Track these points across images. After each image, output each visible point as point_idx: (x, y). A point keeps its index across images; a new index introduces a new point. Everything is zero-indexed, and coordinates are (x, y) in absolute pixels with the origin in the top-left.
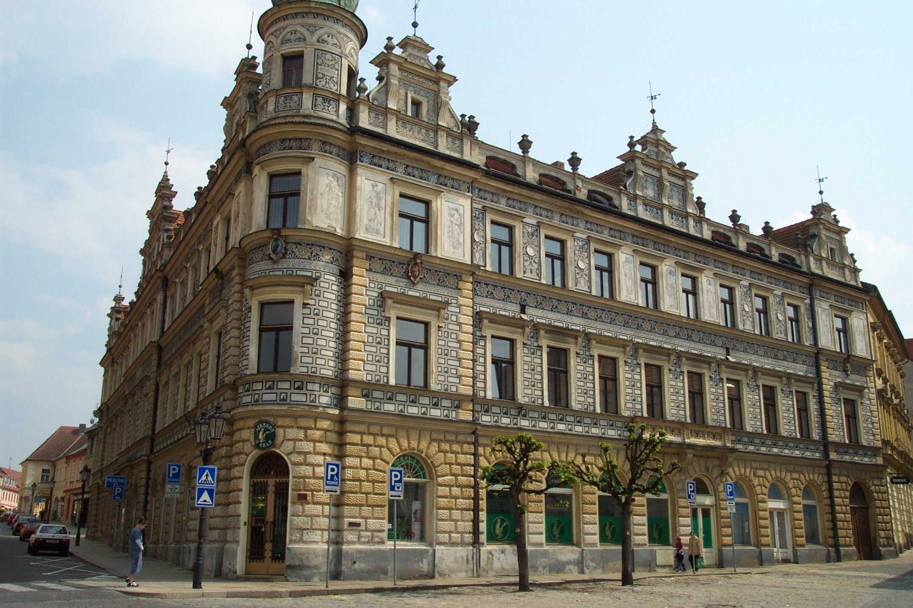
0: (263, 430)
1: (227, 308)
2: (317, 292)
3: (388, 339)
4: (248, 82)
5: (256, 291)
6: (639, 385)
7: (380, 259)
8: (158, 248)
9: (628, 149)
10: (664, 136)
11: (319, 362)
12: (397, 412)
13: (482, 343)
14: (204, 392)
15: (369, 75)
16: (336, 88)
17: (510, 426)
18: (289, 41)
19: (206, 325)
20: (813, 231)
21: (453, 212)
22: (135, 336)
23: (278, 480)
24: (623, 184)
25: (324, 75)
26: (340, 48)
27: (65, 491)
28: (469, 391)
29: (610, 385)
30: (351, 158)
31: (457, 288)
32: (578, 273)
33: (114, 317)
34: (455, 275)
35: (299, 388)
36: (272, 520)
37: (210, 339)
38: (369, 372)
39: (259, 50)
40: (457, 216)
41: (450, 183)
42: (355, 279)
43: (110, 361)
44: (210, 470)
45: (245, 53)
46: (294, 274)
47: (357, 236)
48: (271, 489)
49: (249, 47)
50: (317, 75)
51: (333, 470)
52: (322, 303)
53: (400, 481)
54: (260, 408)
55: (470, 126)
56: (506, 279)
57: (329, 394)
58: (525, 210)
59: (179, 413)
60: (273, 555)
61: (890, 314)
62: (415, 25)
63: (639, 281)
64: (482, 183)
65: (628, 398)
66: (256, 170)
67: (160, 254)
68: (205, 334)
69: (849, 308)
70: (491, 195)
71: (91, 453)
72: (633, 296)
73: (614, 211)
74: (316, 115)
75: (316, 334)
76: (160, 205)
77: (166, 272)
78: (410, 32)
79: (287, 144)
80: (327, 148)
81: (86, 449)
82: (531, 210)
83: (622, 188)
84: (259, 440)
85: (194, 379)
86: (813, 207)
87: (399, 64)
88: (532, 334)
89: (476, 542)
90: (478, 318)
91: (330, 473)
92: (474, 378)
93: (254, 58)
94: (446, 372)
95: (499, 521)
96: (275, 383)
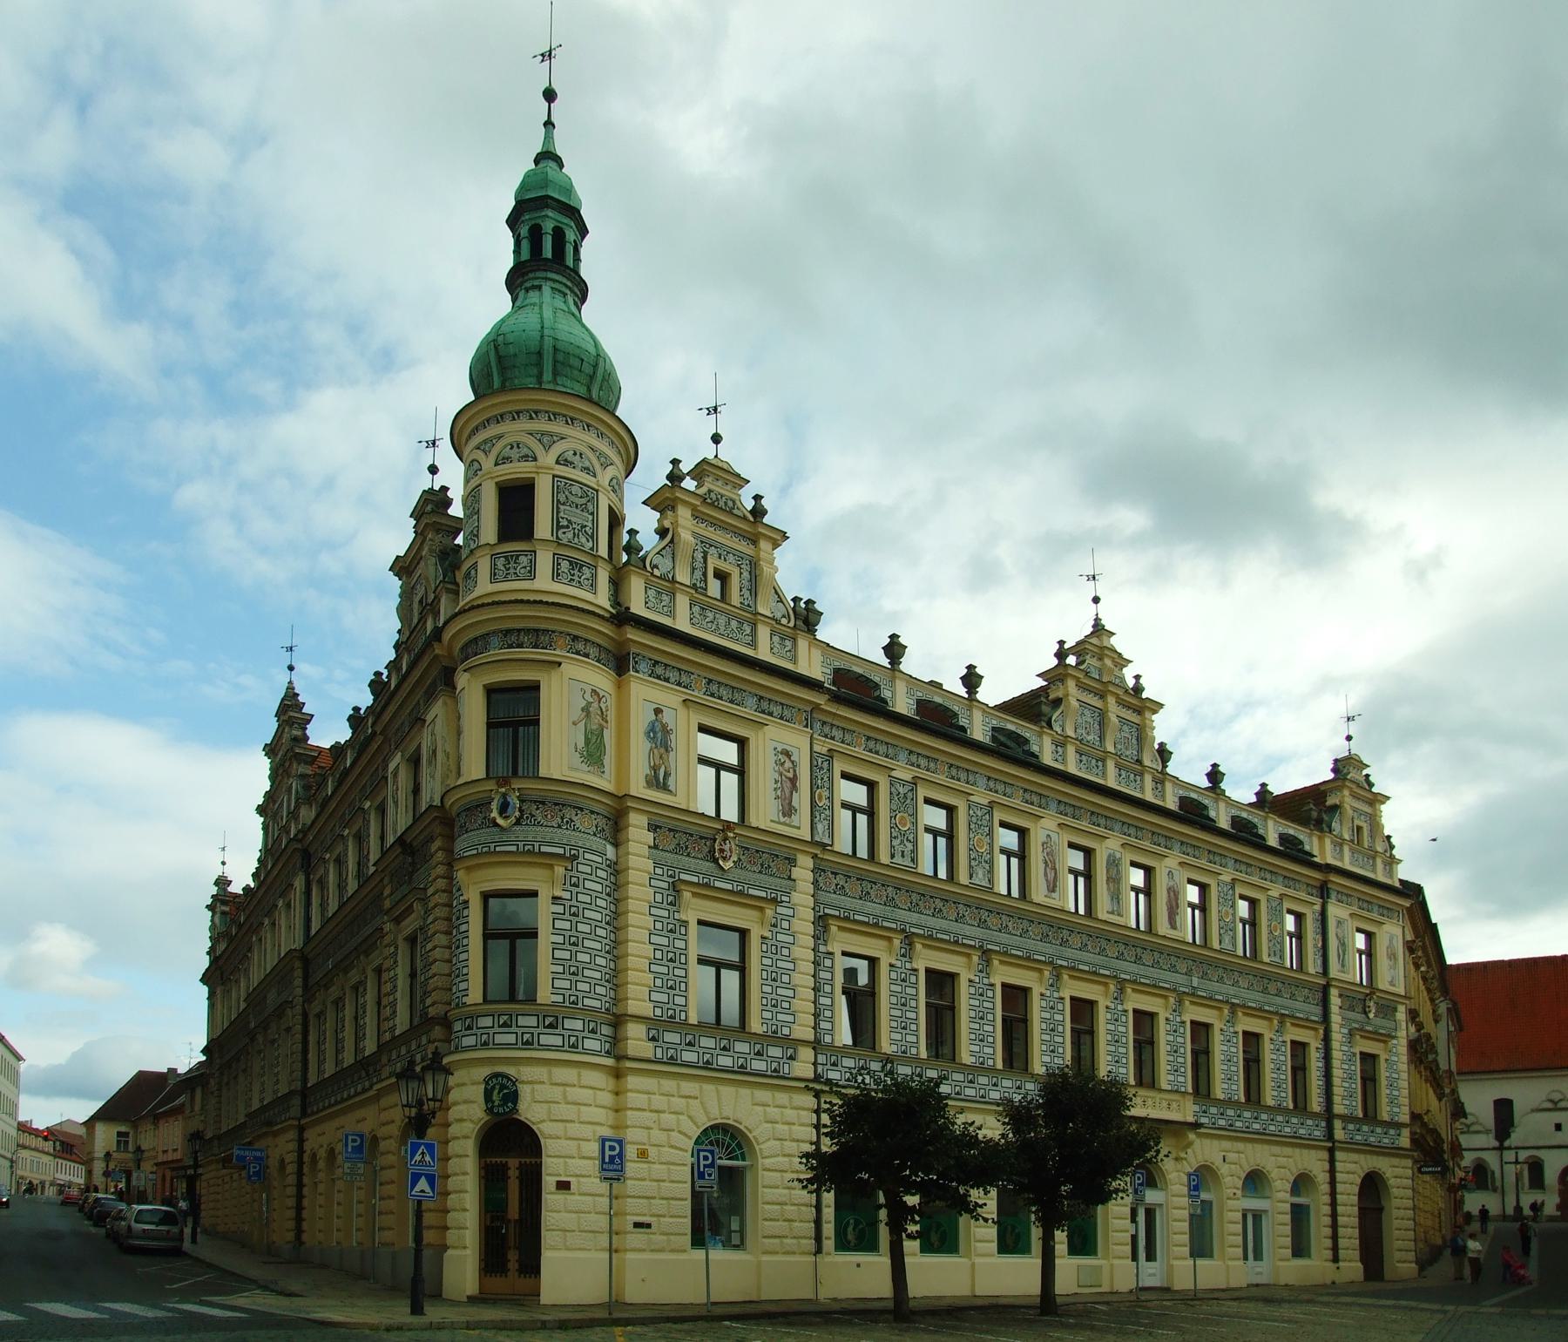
0: (497, 1087)
1: (424, 900)
4: (438, 531)
6: (913, 1003)
9: (1055, 662)
10: (1114, 641)
13: (828, 963)
14: (393, 1028)
15: (642, 522)
16: (590, 544)
17: (840, 1083)
18: (507, 460)
19: (387, 927)
20: (1331, 801)
21: (783, 758)
22: (260, 940)
23: (523, 1160)
24: (1046, 719)
25: (569, 521)
27: (156, 1164)
29: (1202, 1059)
30: (620, 663)
33: (218, 910)
34: (786, 858)
35: (551, 1026)
37: (396, 948)
39: (453, 476)
40: (788, 764)
41: (777, 710)
43: (217, 977)
44: (427, 1146)
45: (426, 482)
46: (537, 850)
48: (513, 1173)
49: (433, 470)
50: (558, 522)
51: (612, 1148)
53: (712, 1165)
55: (807, 617)
59: (348, 1059)
61: (1433, 930)
62: (716, 439)
64: (826, 711)
67: (294, 815)
68: (387, 939)
69: (1379, 918)
70: (841, 732)
73: (1031, 762)
76: (285, 735)
78: (709, 451)
80: (580, 646)
81: (183, 1105)
82: (903, 756)
86: (1336, 761)
87: (694, 509)
88: (903, 950)
89: (819, 1250)
91: (608, 1153)
93: (444, 489)
95: (852, 1221)
96: (514, 1018)
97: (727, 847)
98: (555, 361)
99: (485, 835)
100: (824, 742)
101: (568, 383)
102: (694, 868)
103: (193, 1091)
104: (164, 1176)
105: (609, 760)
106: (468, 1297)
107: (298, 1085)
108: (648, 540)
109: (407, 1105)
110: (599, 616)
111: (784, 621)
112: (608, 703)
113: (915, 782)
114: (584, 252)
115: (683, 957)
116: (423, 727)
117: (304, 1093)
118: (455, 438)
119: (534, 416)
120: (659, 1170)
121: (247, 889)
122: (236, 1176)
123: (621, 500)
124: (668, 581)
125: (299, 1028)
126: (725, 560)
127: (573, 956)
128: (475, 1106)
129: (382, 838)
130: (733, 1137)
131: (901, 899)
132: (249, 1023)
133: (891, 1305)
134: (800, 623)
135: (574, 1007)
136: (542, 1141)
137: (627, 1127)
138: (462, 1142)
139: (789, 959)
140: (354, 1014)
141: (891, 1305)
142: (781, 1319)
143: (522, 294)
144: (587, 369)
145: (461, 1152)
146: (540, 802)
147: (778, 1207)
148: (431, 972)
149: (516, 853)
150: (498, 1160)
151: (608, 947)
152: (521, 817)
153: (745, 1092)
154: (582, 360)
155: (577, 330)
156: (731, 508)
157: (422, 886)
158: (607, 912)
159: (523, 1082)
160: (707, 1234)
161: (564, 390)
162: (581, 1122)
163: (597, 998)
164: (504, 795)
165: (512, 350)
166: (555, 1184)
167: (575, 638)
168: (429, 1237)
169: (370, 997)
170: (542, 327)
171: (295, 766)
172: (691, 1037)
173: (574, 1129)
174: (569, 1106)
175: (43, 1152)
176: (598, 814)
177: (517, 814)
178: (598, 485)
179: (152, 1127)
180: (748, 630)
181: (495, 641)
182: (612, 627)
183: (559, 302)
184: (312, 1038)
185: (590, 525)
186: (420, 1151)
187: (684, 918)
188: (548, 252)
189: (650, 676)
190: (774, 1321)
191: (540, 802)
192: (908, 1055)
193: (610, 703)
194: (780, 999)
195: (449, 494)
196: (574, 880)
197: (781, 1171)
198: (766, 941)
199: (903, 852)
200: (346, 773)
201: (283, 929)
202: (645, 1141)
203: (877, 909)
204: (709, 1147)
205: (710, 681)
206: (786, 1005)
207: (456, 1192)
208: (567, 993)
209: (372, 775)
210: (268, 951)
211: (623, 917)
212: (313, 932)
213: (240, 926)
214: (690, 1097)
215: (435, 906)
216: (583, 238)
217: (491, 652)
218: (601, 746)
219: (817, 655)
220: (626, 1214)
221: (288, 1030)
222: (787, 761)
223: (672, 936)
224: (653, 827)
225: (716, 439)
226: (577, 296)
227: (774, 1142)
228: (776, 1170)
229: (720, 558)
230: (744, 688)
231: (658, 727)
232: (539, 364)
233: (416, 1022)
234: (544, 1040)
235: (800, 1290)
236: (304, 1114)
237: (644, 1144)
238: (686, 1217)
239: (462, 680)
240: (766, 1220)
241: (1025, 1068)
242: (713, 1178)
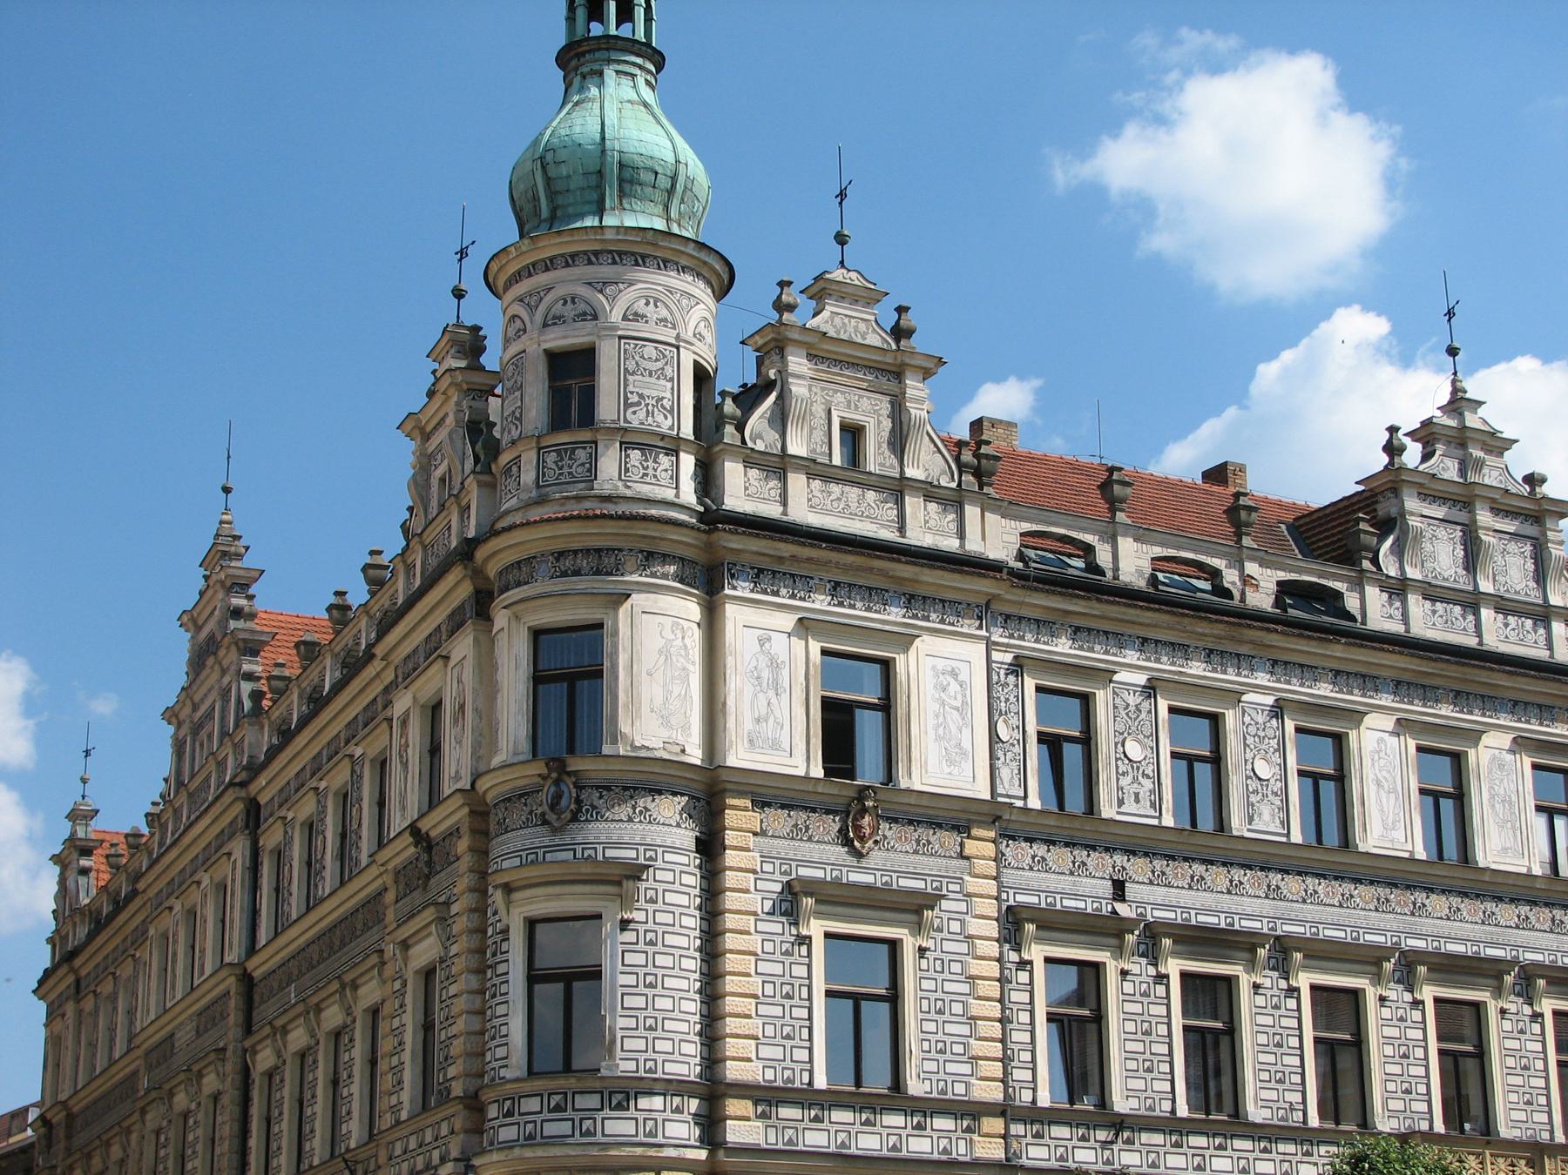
2: (650, 893)
3: (810, 988)
5: (516, 896)
8: (223, 718)
9: (1385, 459)
11: (660, 1045)
12: (833, 1149)
13: (1023, 977)
18: (558, 320)
25: (641, 396)
28: (994, 1093)
29: (1346, 1061)
31: (961, 856)
32: (1256, 792)
37: (404, 984)
38: (769, 1063)
40: (954, 687)
42: (731, 858)
46: (600, 857)
47: (729, 763)
50: (626, 398)
54: (540, 1152)
56: (1077, 824)
57: (686, 1116)
63: (1415, 795)
65: (1391, 1086)
66: (501, 619)
72: (1399, 835)
74: (629, 493)
75: (651, 986)
77: (253, 788)
79: (568, 563)
83: (1366, 564)
90: (1013, 924)
92: (1006, 1060)
94: (942, 1052)
100: (1007, 645)
119: (593, 259)
126: (856, 407)
127: (650, 1003)
143: (577, 80)
154: (656, 173)
165: (564, 170)
181: (544, 568)
184: (256, 1111)
185: (669, 396)
189: (752, 591)
194: (949, 1040)
199: (1137, 795)
222: (953, 682)
226: (649, 72)
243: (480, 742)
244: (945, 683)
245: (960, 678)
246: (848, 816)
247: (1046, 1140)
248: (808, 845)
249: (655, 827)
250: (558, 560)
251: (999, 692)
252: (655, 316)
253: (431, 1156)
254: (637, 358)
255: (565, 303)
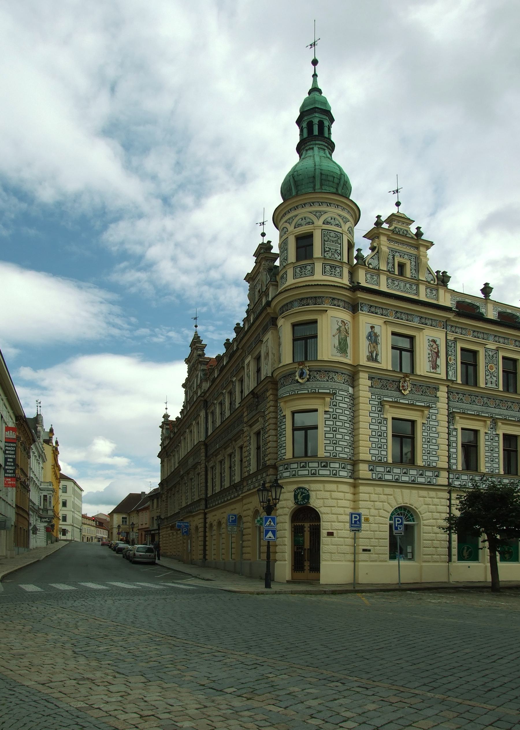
0: (300, 493)
1: (263, 417)
4: (267, 260)
7: (379, 379)
13: (454, 433)
16: (339, 257)
18: (300, 225)
21: (432, 343)
22: (185, 438)
23: (311, 524)
25: (330, 249)
26: (341, 227)
27: (138, 530)
33: (165, 427)
34: (434, 388)
35: (324, 466)
36: (309, 547)
37: (250, 437)
40: (435, 346)
41: (429, 322)
45: (260, 240)
46: (331, 392)
48: (307, 529)
51: (356, 517)
52: (338, 411)
53: (401, 524)
58: (487, 339)
60: (311, 568)
67: (199, 386)
70: (460, 330)
71: (153, 508)
77: (205, 397)
78: (394, 210)
81: (149, 506)
82: (491, 338)
84: (298, 499)
85: (237, 463)
89: (450, 560)
91: (354, 519)
93: (269, 242)
95: (466, 548)
97: (405, 385)
98: (321, 180)
99: (294, 387)
100: (453, 335)
101: (328, 188)
102: (390, 395)
103: (153, 500)
104: (142, 534)
105: (350, 350)
106: (287, 581)
107: (203, 496)
108: (366, 253)
109: (263, 502)
110: (344, 288)
111: (432, 282)
112: (349, 326)
113: (497, 349)
114: (332, 130)
115: (385, 434)
116: (262, 343)
117: (206, 499)
118: (275, 220)
119: (312, 204)
120: (374, 526)
121: (177, 418)
122: (175, 533)
123: (353, 237)
124: (376, 270)
125: (203, 473)
126: (403, 258)
128: (290, 501)
129: (242, 392)
130: (409, 512)
131: (490, 403)
132: (180, 472)
133: (490, 585)
134: (440, 282)
135: (335, 458)
136: (321, 515)
137: (360, 508)
138: (283, 517)
139: (436, 432)
140: (229, 466)
141: (490, 585)
142: (434, 591)
143: (304, 153)
144: (336, 181)
145: (283, 521)
146: (319, 371)
147: (431, 542)
148: (267, 447)
149: (308, 393)
150: (300, 524)
151: (350, 431)
152: (310, 378)
153: (414, 492)
154: (334, 177)
155: (331, 165)
156: (406, 234)
157: (262, 411)
158: (350, 416)
159: (312, 491)
160: (398, 553)
161: (326, 191)
162: (338, 507)
163: (346, 453)
164: (302, 369)
165: (301, 177)
166: (326, 533)
167: (333, 299)
168: (272, 557)
169: (237, 458)
170: (315, 165)
171: (199, 366)
172: (389, 468)
173: (335, 510)
174: (333, 500)
175: (92, 526)
176: (345, 374)
177: (308, 377)
178: (343, 231)
179: (137, 515)
180: (415, 288)
181: (296, 304)
182: (351, 293)
183: (322, 153)
185: (339, 249)
186: (269, 521)
187: (386, 417)
188: (316, 132)
189: (368, 312)
190: (432, 591)
191: (319, 371)
192: (494, 473)
193: (350, 326)
195: (271, 244)
196: (334, 403)
197: (432, 526)
198: (425, 425)
199: (491, 382)
200: (224, 367)
201: (195, 432)
202: (368, 514)
203: (478, 408)
204: (401, 516)
205: (397, 312)
206: (434, 453)
207: (281, 538)
208: (332, 452)
209: (236, 367)
210: (189, 442)
211: (356, 418)
212: (209, 434)
213: (175, 434)
214: (389, 495)
215: (269, 419)
216: (332, 123)
217: (294, 309)
218: (346, 345)
219: (448, 296)
220: (359, 546)
221: (198, 474)
222: (434, 344)
223: (380, 425)
224: (370, 378)
225: (398, 204)
226: (329, 149)
227: (428, 513)
228: (430, 526)
229: (401, 257)
230: (413, 313)
231: (373, 334)
232: (314, 182)
233: (261, 467)
234: (321, 472)
235: (441, 578)
236: (206, 508)
237: (368, 516)
238: (387, 546)
239: (280, 322)
240: (424, 547)
241: (476, 469)
242: (402, 529)
243: (274, 363)
244: (432, 344)
245: (437, 343)
246: (400, 383)
247: (307, 468)
248: (387, 391)
249: (336, 383)
250: (301, 301)
251: (450, 349)
252: (334, 223)
253: (260, 483)
254: (328, 236)
255: (302, 219)
